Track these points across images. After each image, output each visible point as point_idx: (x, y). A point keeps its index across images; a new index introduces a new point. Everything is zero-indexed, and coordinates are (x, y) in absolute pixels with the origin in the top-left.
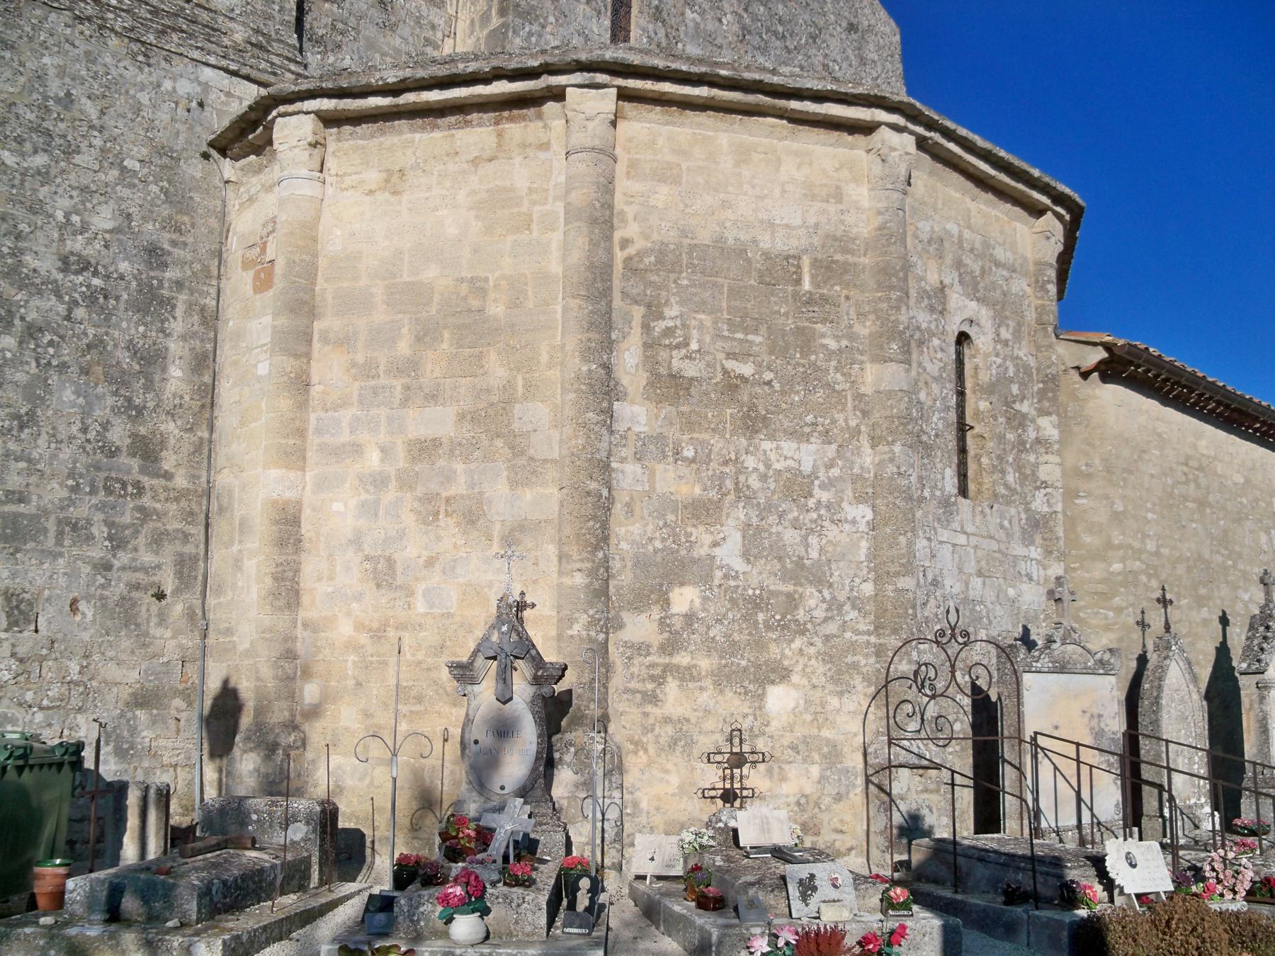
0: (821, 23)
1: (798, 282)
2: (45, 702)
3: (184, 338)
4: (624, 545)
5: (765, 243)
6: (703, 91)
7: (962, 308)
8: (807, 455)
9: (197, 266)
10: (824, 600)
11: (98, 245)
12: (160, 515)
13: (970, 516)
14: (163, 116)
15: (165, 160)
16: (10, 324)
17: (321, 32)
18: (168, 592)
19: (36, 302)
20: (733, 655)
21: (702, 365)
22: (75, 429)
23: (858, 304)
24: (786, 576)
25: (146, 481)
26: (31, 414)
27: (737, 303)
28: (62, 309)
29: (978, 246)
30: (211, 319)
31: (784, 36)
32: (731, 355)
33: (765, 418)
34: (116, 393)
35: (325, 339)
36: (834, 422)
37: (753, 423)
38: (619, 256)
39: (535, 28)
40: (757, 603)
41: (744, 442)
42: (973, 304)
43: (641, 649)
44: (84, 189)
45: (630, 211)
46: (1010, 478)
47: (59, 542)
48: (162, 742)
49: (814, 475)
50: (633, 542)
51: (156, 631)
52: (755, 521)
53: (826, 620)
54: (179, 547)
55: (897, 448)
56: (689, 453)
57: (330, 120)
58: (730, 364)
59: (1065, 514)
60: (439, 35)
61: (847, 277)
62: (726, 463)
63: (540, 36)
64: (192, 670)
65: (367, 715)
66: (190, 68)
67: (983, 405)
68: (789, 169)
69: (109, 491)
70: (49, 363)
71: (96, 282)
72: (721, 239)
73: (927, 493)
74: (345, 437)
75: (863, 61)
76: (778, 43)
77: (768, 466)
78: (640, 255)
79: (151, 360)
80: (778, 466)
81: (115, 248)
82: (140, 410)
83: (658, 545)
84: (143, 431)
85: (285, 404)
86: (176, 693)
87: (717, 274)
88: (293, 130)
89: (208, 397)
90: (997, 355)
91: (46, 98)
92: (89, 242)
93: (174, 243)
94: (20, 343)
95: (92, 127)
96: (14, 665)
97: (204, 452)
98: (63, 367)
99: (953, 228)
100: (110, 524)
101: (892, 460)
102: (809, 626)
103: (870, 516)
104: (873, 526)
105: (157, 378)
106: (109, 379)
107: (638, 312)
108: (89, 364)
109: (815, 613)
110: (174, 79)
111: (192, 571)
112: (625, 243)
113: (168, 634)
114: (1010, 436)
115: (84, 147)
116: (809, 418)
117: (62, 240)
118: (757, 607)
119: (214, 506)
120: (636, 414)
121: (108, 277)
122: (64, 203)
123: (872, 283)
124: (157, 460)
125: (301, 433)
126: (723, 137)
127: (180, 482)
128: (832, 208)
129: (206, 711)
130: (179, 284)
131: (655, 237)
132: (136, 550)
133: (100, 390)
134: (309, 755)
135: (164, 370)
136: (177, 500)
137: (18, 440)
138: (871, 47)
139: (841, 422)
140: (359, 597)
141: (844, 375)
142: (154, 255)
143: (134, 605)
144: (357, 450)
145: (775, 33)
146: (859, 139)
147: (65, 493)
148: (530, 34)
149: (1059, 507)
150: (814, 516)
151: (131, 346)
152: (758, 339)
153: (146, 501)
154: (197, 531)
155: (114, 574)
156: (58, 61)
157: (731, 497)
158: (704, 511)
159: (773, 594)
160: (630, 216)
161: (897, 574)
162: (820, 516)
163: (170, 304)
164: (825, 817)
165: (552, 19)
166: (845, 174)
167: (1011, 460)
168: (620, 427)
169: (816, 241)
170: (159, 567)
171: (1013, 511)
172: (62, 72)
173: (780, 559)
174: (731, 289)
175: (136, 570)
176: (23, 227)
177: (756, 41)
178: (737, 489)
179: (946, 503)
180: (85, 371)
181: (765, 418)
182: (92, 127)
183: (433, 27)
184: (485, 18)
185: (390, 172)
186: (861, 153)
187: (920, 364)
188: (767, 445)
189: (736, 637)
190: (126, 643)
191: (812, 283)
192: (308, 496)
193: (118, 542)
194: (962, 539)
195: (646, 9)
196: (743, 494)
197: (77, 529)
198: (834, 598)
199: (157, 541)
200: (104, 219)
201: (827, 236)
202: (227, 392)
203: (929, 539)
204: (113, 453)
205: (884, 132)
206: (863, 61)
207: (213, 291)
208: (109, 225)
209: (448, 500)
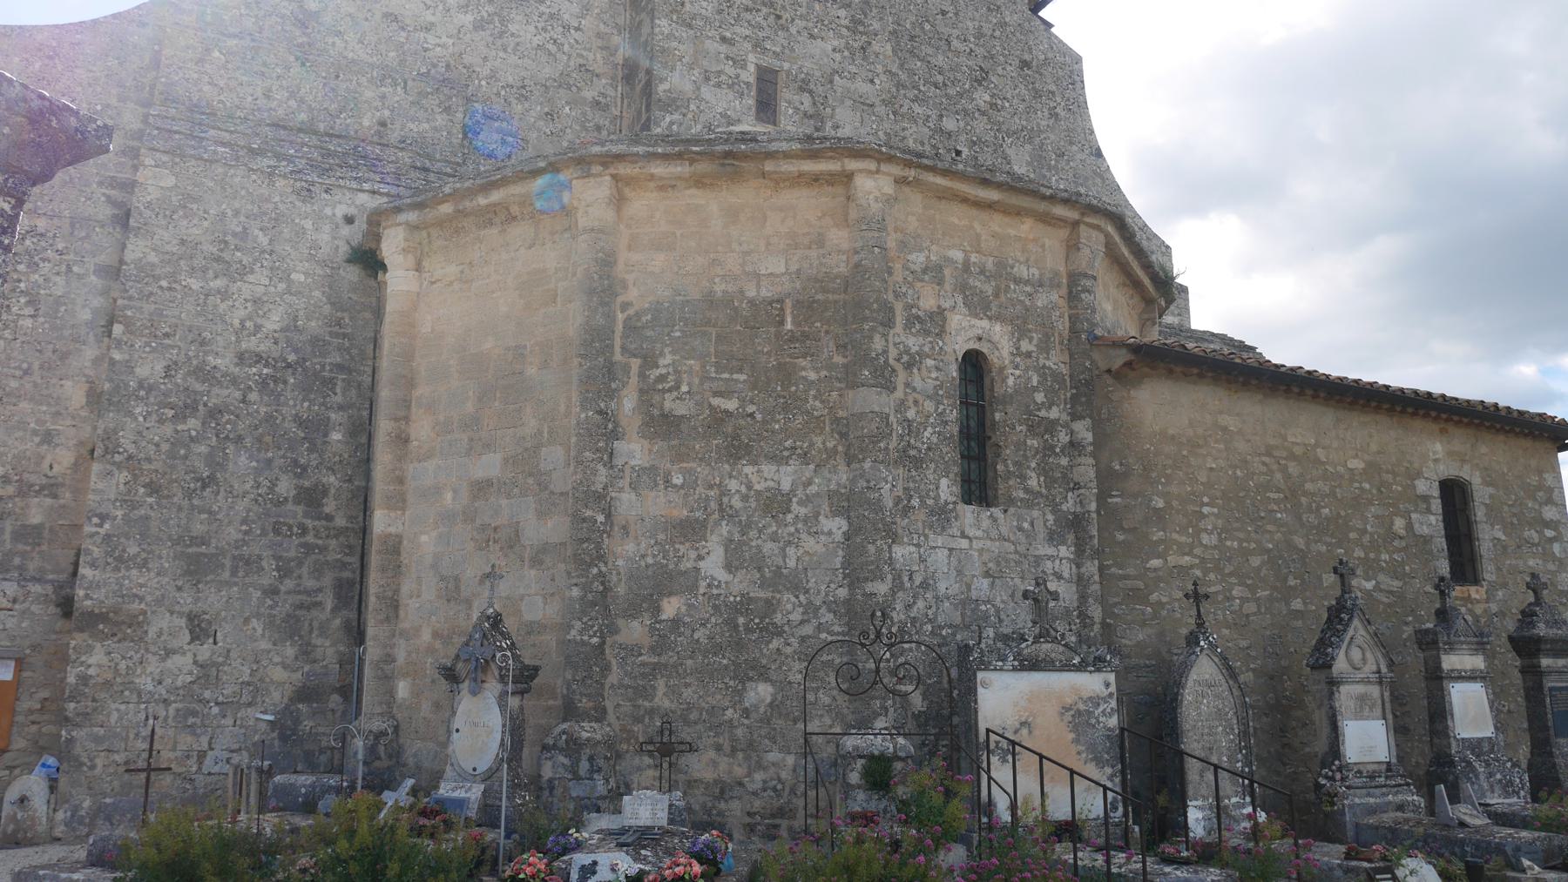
1: (782, 322)
2: (221, 699)
4: (620, 562)
5: (751, 293)
7: (964, 332)
8: (786, 477)
10: (801, 605)
19: (216, 390)
20: (715, 654)
21: (692, 404)
26: (212, 478)
28: (238, 394)
29: (990, 264)
31: (945, 85)
32: (717, 394)
36: (812, 445)
37: (737, 451)
38: (620, 317)
39: (676, 116)
42: (985, 323)
43: (633, 650)
45: (630, 278)
46: (1033, 483)
47: (234, 573)
50: (629, 559)
52: (737, 537)
56: (678, 480)
58: (716, 401)
59: (1098, 513)
62: (711, 487)
69: (277, 532)
70: (227, 437)
77: (749, 488)
78: (638, 315)
80: (757, 487)
83: (650, 560)
90: (1016, 367)
94: (203, 424)
95: (263, 252)
98: (240, 439)
99: (958, 255)
100: (278, 558)
101: (862, 476)
102: (786, 628)
104: (848, 536)
107: (635, 363)
108: (262, 435)
109: (791, 617)
112: (625, 306)
114: (1033, 443)
116: (788, 443)
117: (238, 341)
120: (634, 451)
124: (320, 505)
128: (813, 253)
132: (300, 577)
136: (336, 537)
137: (201, 498)
141: (822, 402)
148: (671, 123)
149: (1093, 506)
150: (792, 529)
151: (297, 419)
152: (743, 377)
157: (716, 516)
158: (691, 530)
162: (797, 530)
167: (1033, 465)
168: (618, 461)
170: (320, 590)
171: (1036, 513)
173: (759, 569)
174: (718, 336)
175: (299, 592)
178: (721, 510)
188: (748, 470)
191: (793, 323)
194: (964, 543)
196: (726, 513)
198: (810, 603)
203: (918, 546)
207: (369, 370)
209: (495, 529)
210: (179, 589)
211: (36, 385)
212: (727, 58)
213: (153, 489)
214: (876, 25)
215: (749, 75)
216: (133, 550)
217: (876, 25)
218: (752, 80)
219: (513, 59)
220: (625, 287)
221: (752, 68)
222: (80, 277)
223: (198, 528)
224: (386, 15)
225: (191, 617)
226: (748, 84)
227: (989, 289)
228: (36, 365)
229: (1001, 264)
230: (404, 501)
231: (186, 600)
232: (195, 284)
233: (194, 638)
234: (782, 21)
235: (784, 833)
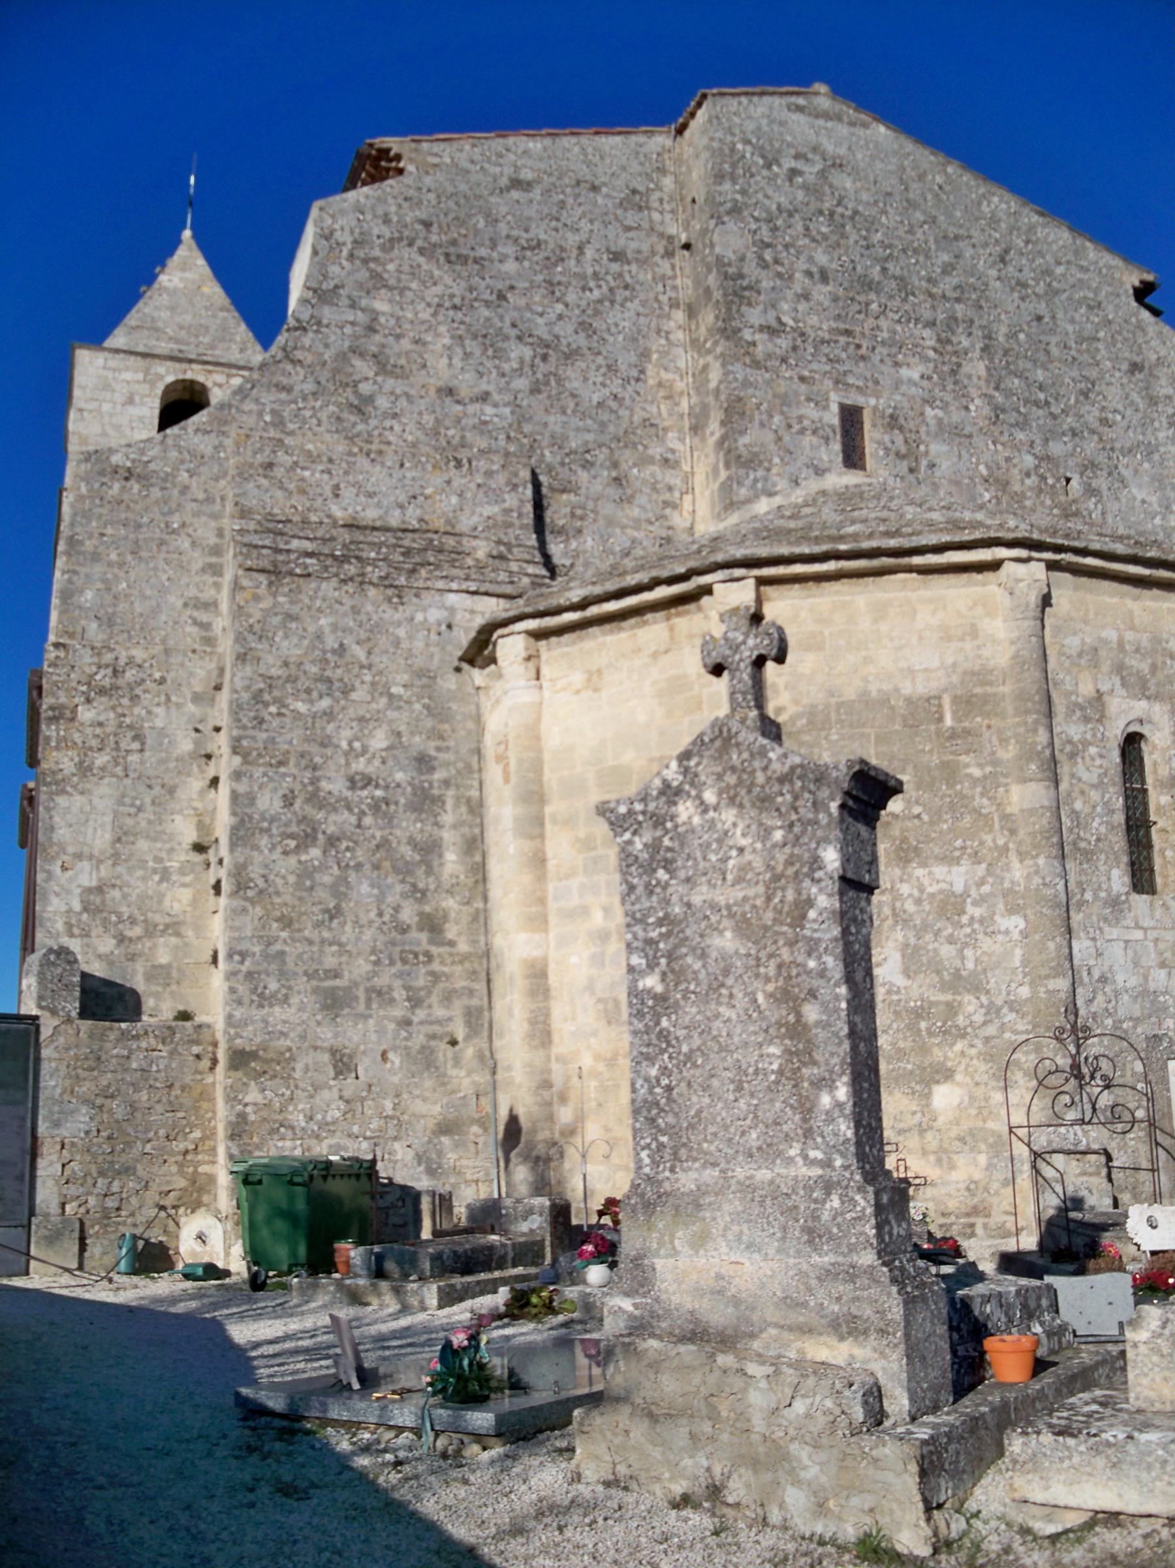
0: (1093, 374)
1: (940, 719)
3: (455, 827)
5: (907, 689)
6: (830, 566)
7: (1124, 712)
8: (958, 877)
9: (460, 765)
11: (377, 762)
12: (448, 977)
13: (1147, 911)
14: (419, 644)
15: (425, 681)
16: (315, 839)
17: (561, 522)
18: (460, 1038)
19: (333, 817)
22: (373, 915)
23: (999, 732)
24: (944, 987)
25: (434, 950)
26: (338, 907)
27: (884, 749)
28: (353, 820)
29: (1145, 643)
30: (476, 808)
31: (1047, 403)
33: (916, 849)
34: (403, 881)
35: (554, 822)
36: (982, 843)
39: (760, 473)
40: (919, 1014)
41: (898, 872)
42: (1143, 704)
44: (361, 719)
48: (464, 1162)
49: (966, 893)
51: (452, 1072)
52: (912, 941)
53: (985, 1023)
54: (465, 1001)
55: (1041, 861)
57: (539, 635)
60: (677, 494)
61: (988, 708)
63: (766, 479)
64: (485, 1102)
65: (607, 1129)
66: (437, 597)
67: (1164, 799)
68: (925, 618)
69: (404, 961)
71: (379, 793)
72: (865, 693)
73: (1088, 896)
74: (575, 901)
75: (1153, 401)
76: (1041, 412)
77: (922, 890)
79: (429, 850)
81: (390, 763)
82: (424, 893)
84: (427, 909)
85: (527, 879)
86: (474, 1121)
87: (864, 725)
88: (511, 647)
89: (480, 874)
91: (324, 652)
92: (369, 761)
93: (438, 749)
95: (362, 667)
96: (342, 1105)
97: (481, 920)
98: (359, 866)
99: (1112, 635)
100: (407, 988)
101: (1037, 872)
103: (1022, 924)
104: (1025, 934)
105: (435, 863)
106: (396, 870)
110: (424, 610)
111: (480, 1020)
113: (463, 1073)
115: (357, 684)
116: (958, 843)
117: (348, 764)
118: (919, 1016)
119: (493, 965)
121: (387, 787)
122: (346, 734)
123: (1010, 710)
125: (542, 901)
126: (860, 597)
127: (463, 947)
128: (968, 645)
129: (500, 1136)
130: (446, 783)
131: (805, 701)
133: (390, 880)
134: (567, 1165)
135: (441, 856)
136: (461, 962)
138: (1163, 382)
139: (990, 843)
140: (595, 1033)
142: (424, 762)
143: (432, 1052)
144: (585, 911)
145: (1036, 403)
146: (989, 576)
147: (369, 967)
148: (756, 480)
151: (411, 841)
153: (436, 966)
154: (481, 986)
155: (414, 1029)
156: (331, 620)
157: (890, 922)
159: (932, 1004)
160: (781, 686)
161: (1047, 977)
163: (440, 800)
164: (995, 1200)
165: (776, 460)
166: (979, 610)
169: (955, 679)
170: (450, 1019)
172: (335, 627)
173: (938, 972)
176: (318, 760)
177: (1012, 417)
178: (895, 914)
179: (1115, 903)
180: (376, 867)
181: (916, 849)
182: (362, 667)
183: (670, 489)
184: (716, 471)
185: (590, 673)
186: (993, 588)
187: (1073, 776)
188: (919, 872)
189: (901, 1044)
190: (428, 1083)
192: (552, 955)
193: (415, 1002)
194: (1138, 935)
195: (879, 421)
197: (381, 995)
198: (991, 1003)
199: (448, 998)
200: (379, 741)
201: (965, 673)
202: (495, 869)
203: (1094, 939)
204: (404, 930)
205: (1008, 567)
206: (1153, 401)
207: (476, 784)
208: (384, 745)
210: (319, 1023)
211: (150, 822)
212: (809, 400)
213: (286, 922)
214: (965, 343)
215: (832, 417)
216: (273, 986)
217: (965, 343)
218: (836, 421)
219: (576, 422)
220: (777, 692)
221: (835, 408)
222: (179, 706)
223: (330, 962)
224: (439, 390)
225: (333, 1052)
226: (832, 427)
227: (1145, 667)
228: (148, 800)
229: (1156, 640)
230: (546, 922)
231: (326, 1035)
232: (301, 707)
233: (338, 1073)
234: (863, 351)
235: (979, 1230)
